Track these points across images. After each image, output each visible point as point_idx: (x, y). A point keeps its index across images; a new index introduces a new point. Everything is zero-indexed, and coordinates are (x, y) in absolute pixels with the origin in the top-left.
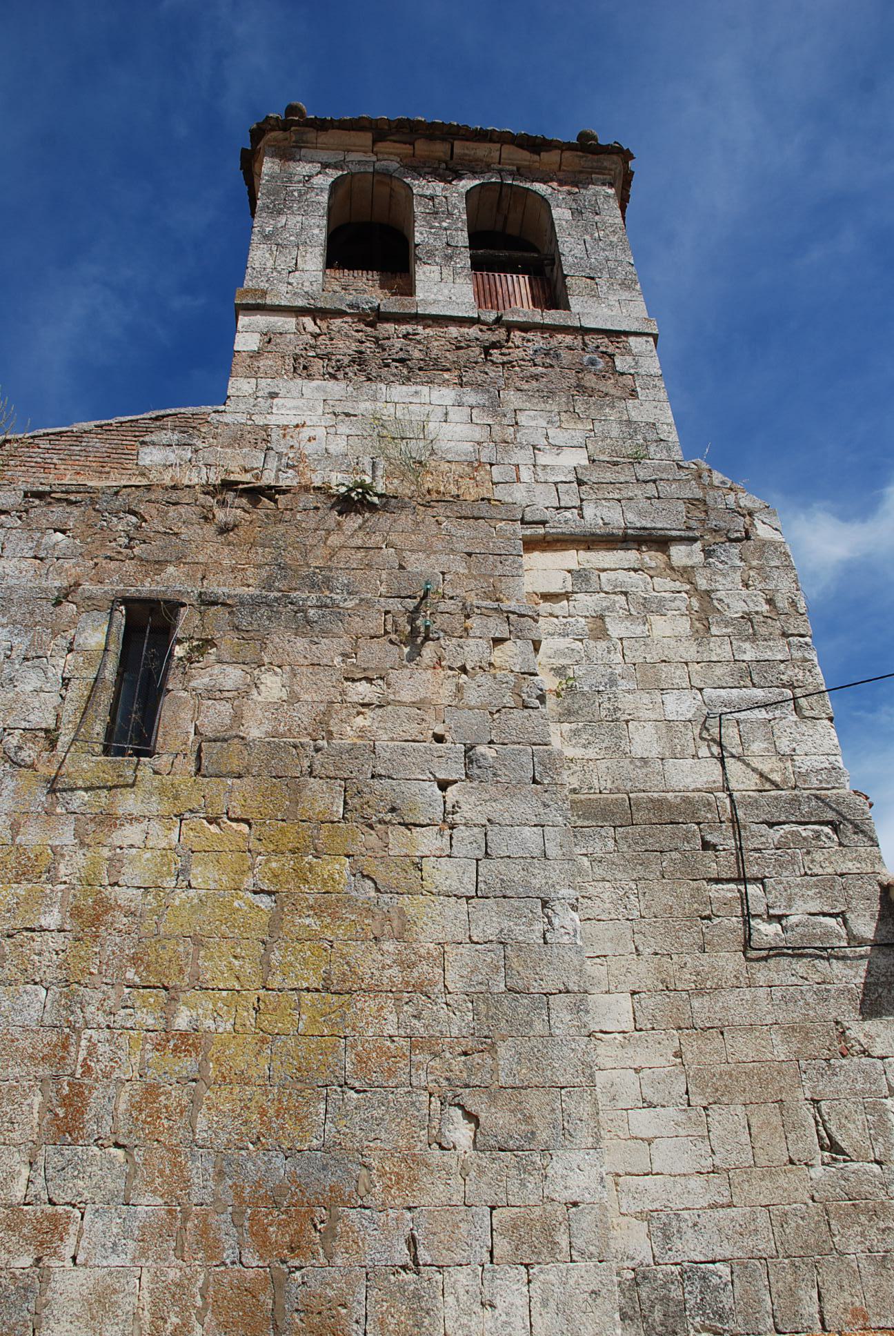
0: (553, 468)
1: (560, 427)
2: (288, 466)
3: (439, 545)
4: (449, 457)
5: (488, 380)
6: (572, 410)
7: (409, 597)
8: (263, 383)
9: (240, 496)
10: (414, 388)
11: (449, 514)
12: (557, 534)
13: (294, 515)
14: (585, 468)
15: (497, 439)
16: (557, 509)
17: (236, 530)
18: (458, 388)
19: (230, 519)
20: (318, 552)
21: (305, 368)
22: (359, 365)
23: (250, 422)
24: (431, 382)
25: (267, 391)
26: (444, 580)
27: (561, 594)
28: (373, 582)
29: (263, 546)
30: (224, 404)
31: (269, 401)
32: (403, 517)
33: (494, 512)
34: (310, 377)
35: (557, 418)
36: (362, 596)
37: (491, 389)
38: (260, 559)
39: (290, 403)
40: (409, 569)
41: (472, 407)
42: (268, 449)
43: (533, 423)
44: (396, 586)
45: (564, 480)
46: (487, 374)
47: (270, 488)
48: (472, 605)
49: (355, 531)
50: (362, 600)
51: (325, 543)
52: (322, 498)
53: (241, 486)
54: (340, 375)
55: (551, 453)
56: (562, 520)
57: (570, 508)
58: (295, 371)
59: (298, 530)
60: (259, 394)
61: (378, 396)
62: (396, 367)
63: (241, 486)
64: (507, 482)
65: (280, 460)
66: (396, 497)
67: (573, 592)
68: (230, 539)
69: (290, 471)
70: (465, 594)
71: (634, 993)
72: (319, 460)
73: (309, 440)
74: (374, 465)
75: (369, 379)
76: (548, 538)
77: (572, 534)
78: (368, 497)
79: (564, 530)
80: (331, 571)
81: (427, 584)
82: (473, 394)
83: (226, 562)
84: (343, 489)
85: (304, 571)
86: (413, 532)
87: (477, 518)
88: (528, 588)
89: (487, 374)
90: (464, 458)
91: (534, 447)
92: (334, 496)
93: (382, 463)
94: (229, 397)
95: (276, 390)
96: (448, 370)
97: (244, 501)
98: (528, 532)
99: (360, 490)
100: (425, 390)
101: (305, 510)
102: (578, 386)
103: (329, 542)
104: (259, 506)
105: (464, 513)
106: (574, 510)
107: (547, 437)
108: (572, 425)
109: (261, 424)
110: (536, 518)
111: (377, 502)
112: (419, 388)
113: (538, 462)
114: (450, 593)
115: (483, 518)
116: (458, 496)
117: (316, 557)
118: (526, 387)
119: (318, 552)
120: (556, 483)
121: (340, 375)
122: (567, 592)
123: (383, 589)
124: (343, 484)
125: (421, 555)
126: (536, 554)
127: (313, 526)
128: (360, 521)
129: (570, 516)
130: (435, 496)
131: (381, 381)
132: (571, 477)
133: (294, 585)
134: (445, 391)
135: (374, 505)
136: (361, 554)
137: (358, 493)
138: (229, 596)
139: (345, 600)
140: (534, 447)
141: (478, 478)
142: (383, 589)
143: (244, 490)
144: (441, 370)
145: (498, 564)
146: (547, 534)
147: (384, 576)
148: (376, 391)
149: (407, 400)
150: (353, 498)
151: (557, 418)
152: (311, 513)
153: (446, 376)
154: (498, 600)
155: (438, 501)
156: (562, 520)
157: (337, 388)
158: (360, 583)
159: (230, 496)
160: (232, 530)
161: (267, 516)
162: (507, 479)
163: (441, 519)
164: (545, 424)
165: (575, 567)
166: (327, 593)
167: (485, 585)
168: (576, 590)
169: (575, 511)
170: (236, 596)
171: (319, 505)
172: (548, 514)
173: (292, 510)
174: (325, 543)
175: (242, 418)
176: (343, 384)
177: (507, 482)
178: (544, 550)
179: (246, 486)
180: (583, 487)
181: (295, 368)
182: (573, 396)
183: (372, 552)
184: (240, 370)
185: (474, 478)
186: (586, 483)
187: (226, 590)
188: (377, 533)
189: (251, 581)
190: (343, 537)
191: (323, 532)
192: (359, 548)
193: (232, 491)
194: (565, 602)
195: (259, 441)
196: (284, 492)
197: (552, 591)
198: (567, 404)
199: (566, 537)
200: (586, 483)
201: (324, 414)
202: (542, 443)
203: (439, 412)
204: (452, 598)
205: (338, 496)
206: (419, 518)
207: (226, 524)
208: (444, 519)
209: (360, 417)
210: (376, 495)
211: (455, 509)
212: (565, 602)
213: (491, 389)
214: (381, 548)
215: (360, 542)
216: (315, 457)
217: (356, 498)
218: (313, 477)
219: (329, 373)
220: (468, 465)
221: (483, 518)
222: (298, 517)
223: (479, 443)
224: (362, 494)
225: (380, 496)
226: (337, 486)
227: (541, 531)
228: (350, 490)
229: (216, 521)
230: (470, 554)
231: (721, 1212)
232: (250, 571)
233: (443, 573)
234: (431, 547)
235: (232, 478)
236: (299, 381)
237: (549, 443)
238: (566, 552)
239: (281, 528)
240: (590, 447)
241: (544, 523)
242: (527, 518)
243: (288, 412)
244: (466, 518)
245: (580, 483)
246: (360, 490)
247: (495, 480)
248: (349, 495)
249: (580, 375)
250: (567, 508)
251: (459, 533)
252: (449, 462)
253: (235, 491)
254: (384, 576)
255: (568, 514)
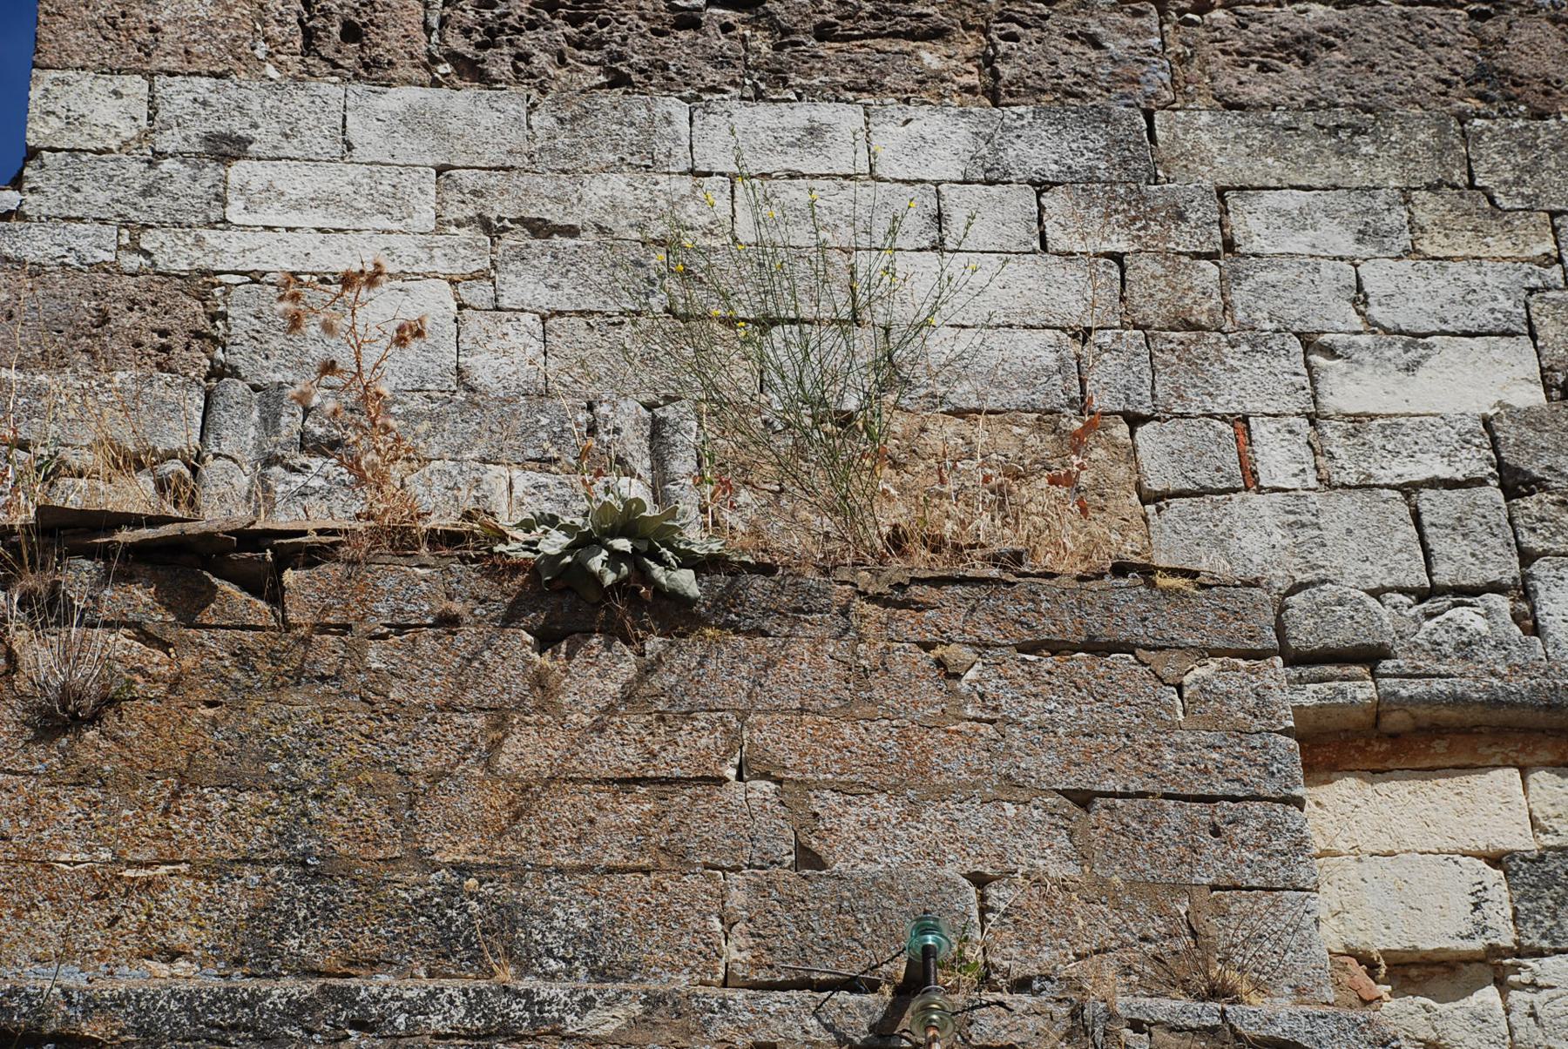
0: (1392, 424)
1: (1412, 252)
2: (308, 444)
3: (955, 762)
4: (964, 394)
5: (1102, 71)
6: (1459, 176)
7: (851, 985)
8: (179, 95)
9: (125, 577)
10: (800, 115)
11: (987, 633)
12: (1432, 701)
13: (355, 653)
14: (1530, 418)
15: (1150, 312)
16: (1422, 595)
17: (111, 718)
18: (980, 108)
19: (86, 674)
20: (464, 804)
21: (352, 32)
22: (574, 21)
23: (132, 261)
24: (872, 87)
25: (198, 128)
26: (983, 911)
27: (1470, 960)
28: (694, 922)
29: (233, 783)
30: (17, 183)
31: (210, 172)
32: (801, 648)
33: (1169, 623)
34: (374, 71)
35: (1398, 217)
36: (653, 985)
37: (1118, 109)
38: (220, 842)
39: (297, 181)
40: (839, 866)
41: (1042, 186)
42: (218, 372)
43: (1298, 243)
44: (789, 937)
45: (1444, 472)
46: (1095, 43)
47: (251, 539)
48: (1112, 1016)
49: (610, 709)
50: (654, 1001)
51: (489, 766)
52: (469, 578)
53: (125, 536)
54: (499, 64)
55: (1381, 362)
56: (1448, 640)
57: (1476, 591)
58: (309, 46)
59: (375, 715)
60: (168, 142)
61: (661, 149)
62: (726, 28)
63: (125, 536)
64: (1202, 492)
65: (270, 422)
66: (767, 570)
67: (1521, 951)
68: (88, 756)
69: (316, 463)
70: (1074, 969)
71: (440, 170)
72: (436, 418)
73: (400, 341)
74: (657, 432)
75: (618, 81)
76: (1395, 720)
77: (1495, 703)
78: (658, 571)
79: (1461, 686)
80: (519, 880)
81: (923, 930)
82: (1041, 130)
83: (71, 855)
84: (554, 543)
85: (408, 885)
86: (847, 711)
87: (1098, 648)
88: (1331, 936)
89: (1095, 43)
90: (1020, 396)
91: (1309, 343)
92: (516, 568)
93: (688, 435)
94: (33, 153)
95: (239, 127)
96: (937, 34)
97: (141, 596)
98: (1309, 696)
99: (623, 544)
100: (844, 118)
101: (400, 629)
102: (1482, 74)
103: (504, 760)
104: (206, 617)
105: (1046, 629)
106: (1494, 600)
107: (1359, 296)
108: (1464, 244)
109: (182, 265)
110: (1340, 637)
111: (694, 590)
112: (824, 112)
113: (1330, 403)
114: (1012, 959)
115: (1128, 647)
116: (1017, 557)
117: (454, 826)
118: (1261, 91)
119: (464, 804)
120: (1409, 489)
121: (499, 64)
122: (1494, 951)
123: (736, 952)
124: (552, 521)
125: (886, 807)
126: (1346, 788)
127: (433, 696)
128: (627, 668)
129: (1481, 625)
130: (921, 560)
131: (668, 86)
132: (1474, 462)
133: (366, 944)
134: (928, 121)
135: (683, 601)
136: (636, 808)
137: (616, 557)
138: (92, 1006)
139: (587, 1004)
140: (1309, 343)
141: (1085, 479)
142: (736, 952)
143: (140, 551)
144: (910, 35)
145: (1205, 838)
146: (1387, 702)
147: (738, 898)
148: (648, 130)
149: (776, 163)
150: (596, 579)
151: (1398, 217)
152: (427, 644)
153: (931, 57)
154: (1216, 992)
155: (937, 582)
156: (1448, 640)
157: (487, 118)
158: (643, 929)
159: (78, 577)
160: (94, 719)
161: (242, 656)
162: (1203, 478)
163: (956, 653)
164: (1345, 244)
165: (1520, 839)
166: (507, 975)
167: (1156, 927)
168: (1535, 940)
169: (1502, 603)
170: (119, 1002)
171: (457, 607)
172: (1388, 619)
173: (346, 628)
174: (489, 766)
175: (97, 244)
176: (512, 102)
177: (1202, 492)
178: (1377, 771)
179: (146, 533)
180: (1530, 504)
181: (309, 35)
182: (1462, 118)
183: (682, 798)
184: (74, 38)
185: (1069, 480)
186: (1540, 484)
187: (73, 977)
188: (702, 720)
189: (182, 935)
190: (560, 739)
191: (480, 722)
192: (627, 782)
193: (90, 553)
194: (1490, 994)
195: (178, 339)
196: (311, 556)
197: (1429, 946)
198: (1439, 153)
199: (1471, 716)
200: (1540, 484)
201: (441, 224)
202: (1340, 320)
203: (914, 210)
204: (1022, 985)
205: (534, 570)
206: (868, 654)
207: (67, 693)
208: (967, 654)
209: (589, 238)
210: (689, 560)
211: (1012, 611)
212: (1490, 994)
213: (1118, 109)
214: (721, 781)
215: (630, 758)
216: (417, 403)
217: (610, 578)
218: (416, 487)
219: (454, 57)
220: (1039, 426)
221: (1128, 647)
222: (374, 657)
223: (1082, 335)
224: (633, 558)
225: (703, 565)
226: (527, 526)
227: (1364, 691)
228: (584, 542)
229: (22, 684)
230: (1083, 799)
231: (529, 296)
232: (179, 891)
233: (979, 880)
234: (921, 771)
235: (74, 496)
236: (330, 89)
237: (1373, 326)
238: (1475, 779)
239: (304, 704)
240: (1548, 330)
241: (1370, 656)
242: (1303, 635)
243: (293, 219)
244: (1056, 648)
245: (1515, 483)
246: (623, 544)
247: (1155, 484)
248: (580, 567)
249: (1491, 29)
250: (1464, 593)
251: (1035, 710)
252: (959, 413)
253: (105, 553)
254: (738, 898)
255: (1469, 617)
